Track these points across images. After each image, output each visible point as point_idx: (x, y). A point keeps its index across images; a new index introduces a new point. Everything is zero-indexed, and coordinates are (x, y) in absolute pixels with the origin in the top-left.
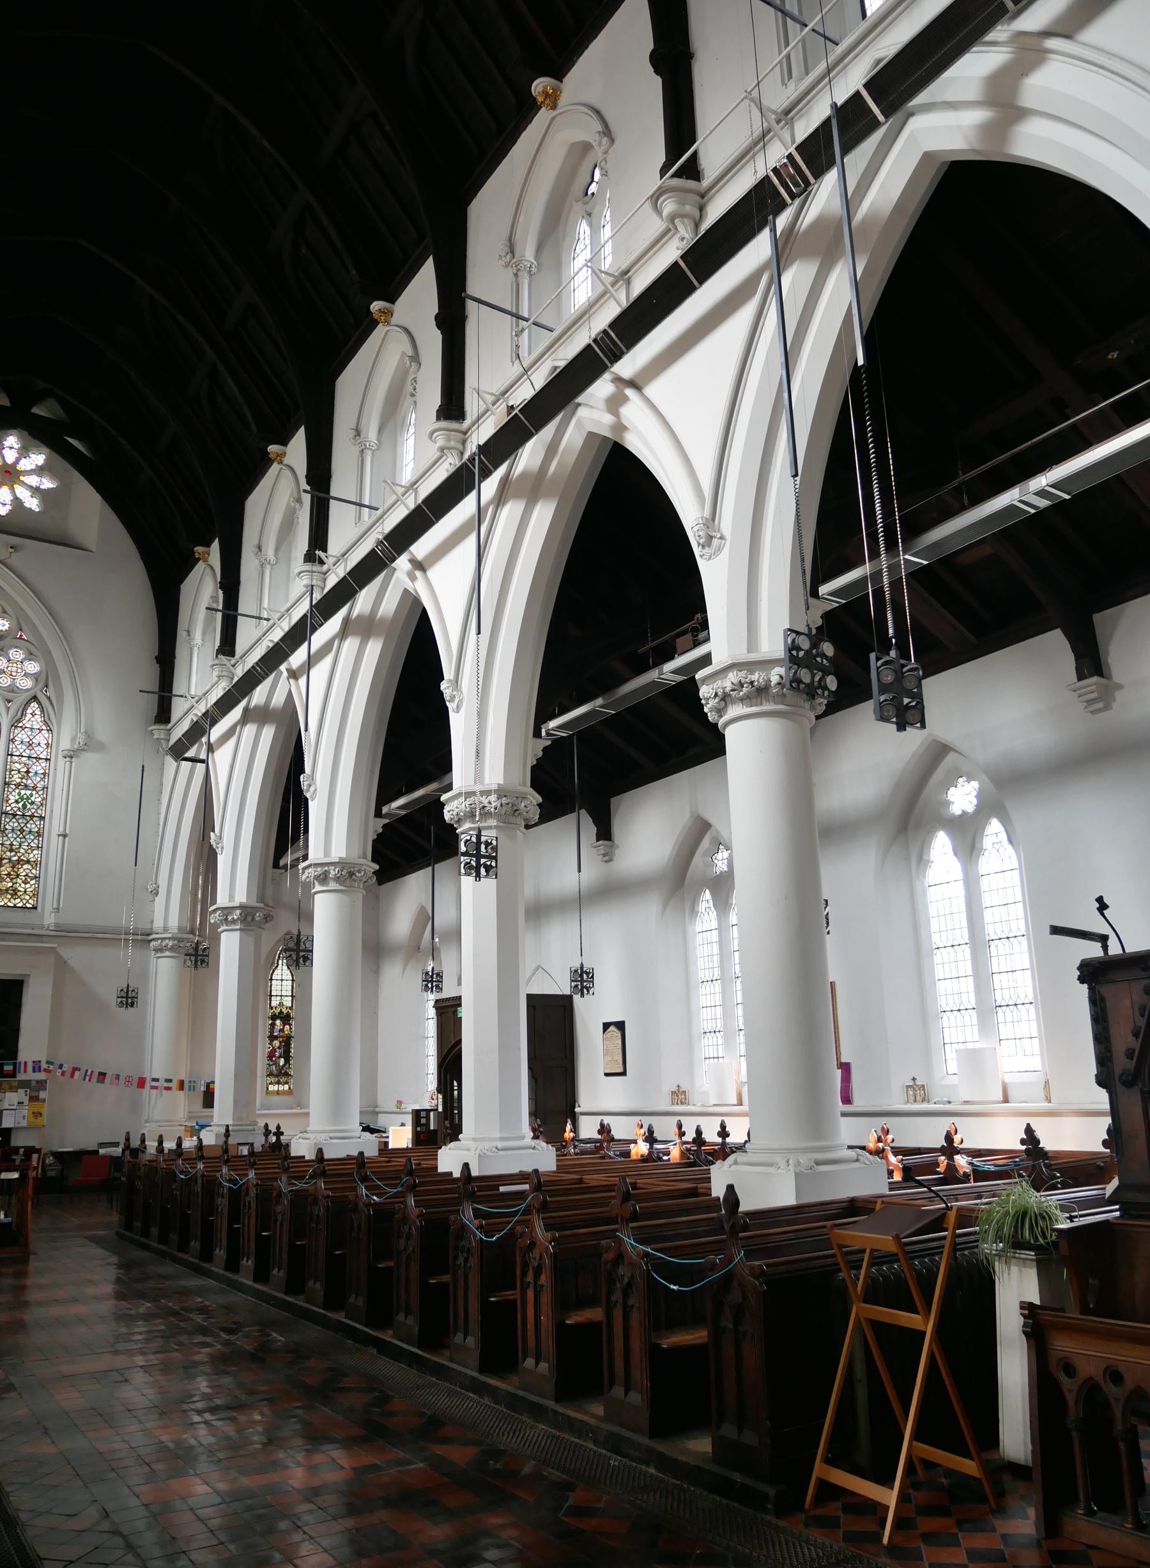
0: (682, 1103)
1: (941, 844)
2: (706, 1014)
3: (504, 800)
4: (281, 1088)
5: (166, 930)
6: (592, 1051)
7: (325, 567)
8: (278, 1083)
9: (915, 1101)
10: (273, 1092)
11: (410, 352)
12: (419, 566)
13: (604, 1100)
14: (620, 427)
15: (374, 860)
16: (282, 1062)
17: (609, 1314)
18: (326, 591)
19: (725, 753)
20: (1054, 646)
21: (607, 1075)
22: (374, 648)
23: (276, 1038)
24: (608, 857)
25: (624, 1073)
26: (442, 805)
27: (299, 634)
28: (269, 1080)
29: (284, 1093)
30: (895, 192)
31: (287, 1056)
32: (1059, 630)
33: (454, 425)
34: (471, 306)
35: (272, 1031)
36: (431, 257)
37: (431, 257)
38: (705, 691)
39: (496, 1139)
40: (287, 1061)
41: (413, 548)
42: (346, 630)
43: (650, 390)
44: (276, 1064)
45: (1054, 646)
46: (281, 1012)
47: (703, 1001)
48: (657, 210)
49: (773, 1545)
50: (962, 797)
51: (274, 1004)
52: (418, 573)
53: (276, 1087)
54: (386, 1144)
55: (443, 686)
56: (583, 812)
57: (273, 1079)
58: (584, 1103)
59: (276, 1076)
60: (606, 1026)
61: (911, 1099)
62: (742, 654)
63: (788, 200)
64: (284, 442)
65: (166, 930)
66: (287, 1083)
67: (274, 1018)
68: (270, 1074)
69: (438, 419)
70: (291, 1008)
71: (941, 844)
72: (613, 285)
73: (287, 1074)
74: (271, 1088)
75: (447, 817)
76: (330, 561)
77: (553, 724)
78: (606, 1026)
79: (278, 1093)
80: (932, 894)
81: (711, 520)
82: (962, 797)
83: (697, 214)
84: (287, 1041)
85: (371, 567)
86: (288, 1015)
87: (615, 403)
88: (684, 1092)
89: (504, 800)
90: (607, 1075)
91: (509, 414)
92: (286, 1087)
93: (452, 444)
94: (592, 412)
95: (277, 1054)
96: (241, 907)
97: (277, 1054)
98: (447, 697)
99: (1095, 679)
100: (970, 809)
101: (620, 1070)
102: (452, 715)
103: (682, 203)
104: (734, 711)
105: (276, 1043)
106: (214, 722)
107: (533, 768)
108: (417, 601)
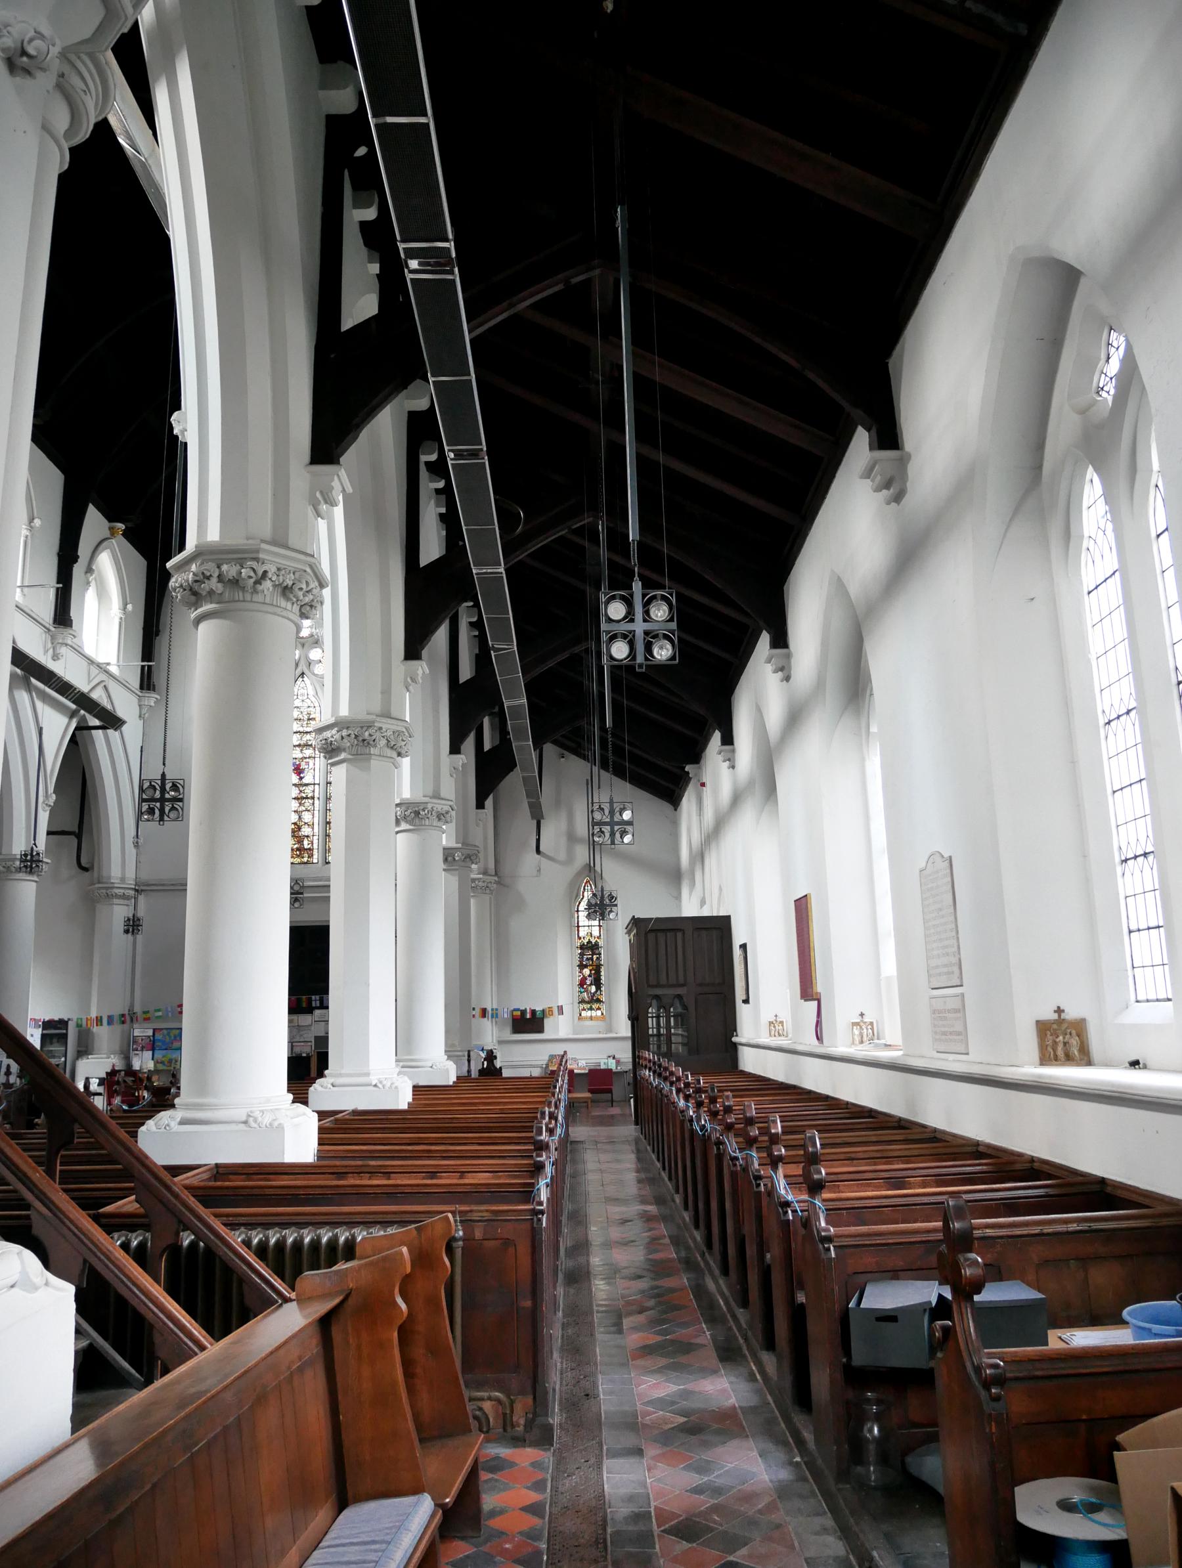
0: (1069, 1059)
3: (345, 733)
4: (594, 1013)
5: (123, 879)
8: (591, 1009)
9: (862, 1042)
10: (586, 1018)
16: (593, 989)
23: (586, 966)
28: (582, 1006)
29: (597, 1018)
31: (597, 982)
35: (581, 962)
36: (91, 509)
37: (91, 509)
40: (598, 987)
44: (586, 990)
46: (589, 942)
51: (582, 934)
53: (589, 1013)
54: (598, 1081)
57: (587, 1006)
59: (588, 1003)
61: (857, 1039)
63: (450, 277)
65: (123, 879)
66: (599, 1009)
67: (582, 947)
68: (582, 1001)
70: (599, 937)
73: (599, 1001)
74: (584, 1014)
79: (591, 1018)
84: (597, 970)
86: (597, 944)
88: (782, 1022)
89: (345, 733)
92: (599, 1013)
95: (588, 982)
97: (588, 982)
105: (586, 972)
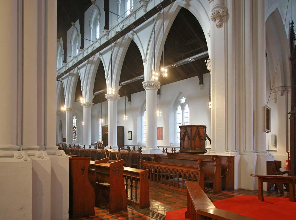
1: (179, 107)
2: (144, 131)
6: (127, 136)
7: (84, 50)
11: (99, 13)
12: (101, 54)
13: (128, 142)
14: (133, 38)
15: (93, 102)
16: (75, 135)
17: (127, 163)
18: (88, 60)
19: (123, 127)
20: (197, 78)
21: (129, 139)
22: (93, 66)
24: (130, 104)
25: (131, 139)
26: (105, 96)
27: (81, 62)
30: (174, 10)
32: (197, 76)
33: (107, 30)
34: (109, 13)
38: (143, 85)
39: (113, 146)
41: (100, 51)
42: (88, 63)
43: (138, 34)
45: (197, 78)
47: (144, 129)
48: (141, 4)
49: (152, 215)
50: (183, 100)
52: (101, 56)
55: (105, 77)
56: (126, 96)
58: (125, 144)
60: (129, 132)
62: (149, 80)
64: (75, 22)
69: (104, 29)
71: (179, 107)
72: (133, 13)
75: (106, 98)
76: (85, 49)
77: (122, 83)
78: (129, 132)
80: (144, 119)
81: (145, 59)
82: (183, 100)
83: (146, 5)
85: (93, 53)
87: (133, 34)
90: (129, 139)
91: (117, 33)
93: (107, 34)
94: (129, 35)
96: (70, 108)
98: (106, 78)
99: (202, 85)
100: (184, 102)
101: (131, 139)
102: (107, 81)
103: (144, 3)
104: (147, 88)
106: (63, 75)
107: (119, 91)
108: (100, 59)
